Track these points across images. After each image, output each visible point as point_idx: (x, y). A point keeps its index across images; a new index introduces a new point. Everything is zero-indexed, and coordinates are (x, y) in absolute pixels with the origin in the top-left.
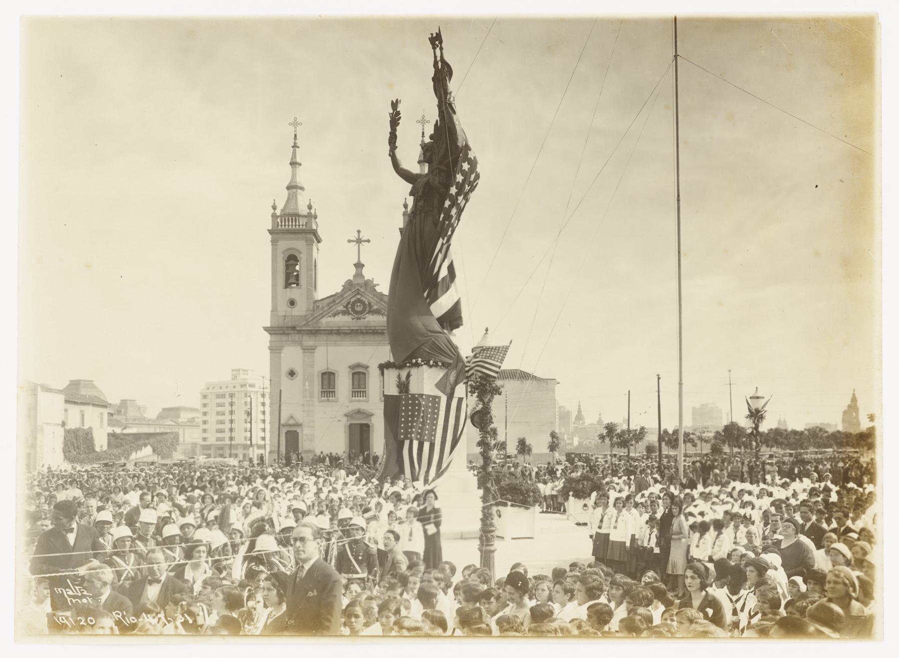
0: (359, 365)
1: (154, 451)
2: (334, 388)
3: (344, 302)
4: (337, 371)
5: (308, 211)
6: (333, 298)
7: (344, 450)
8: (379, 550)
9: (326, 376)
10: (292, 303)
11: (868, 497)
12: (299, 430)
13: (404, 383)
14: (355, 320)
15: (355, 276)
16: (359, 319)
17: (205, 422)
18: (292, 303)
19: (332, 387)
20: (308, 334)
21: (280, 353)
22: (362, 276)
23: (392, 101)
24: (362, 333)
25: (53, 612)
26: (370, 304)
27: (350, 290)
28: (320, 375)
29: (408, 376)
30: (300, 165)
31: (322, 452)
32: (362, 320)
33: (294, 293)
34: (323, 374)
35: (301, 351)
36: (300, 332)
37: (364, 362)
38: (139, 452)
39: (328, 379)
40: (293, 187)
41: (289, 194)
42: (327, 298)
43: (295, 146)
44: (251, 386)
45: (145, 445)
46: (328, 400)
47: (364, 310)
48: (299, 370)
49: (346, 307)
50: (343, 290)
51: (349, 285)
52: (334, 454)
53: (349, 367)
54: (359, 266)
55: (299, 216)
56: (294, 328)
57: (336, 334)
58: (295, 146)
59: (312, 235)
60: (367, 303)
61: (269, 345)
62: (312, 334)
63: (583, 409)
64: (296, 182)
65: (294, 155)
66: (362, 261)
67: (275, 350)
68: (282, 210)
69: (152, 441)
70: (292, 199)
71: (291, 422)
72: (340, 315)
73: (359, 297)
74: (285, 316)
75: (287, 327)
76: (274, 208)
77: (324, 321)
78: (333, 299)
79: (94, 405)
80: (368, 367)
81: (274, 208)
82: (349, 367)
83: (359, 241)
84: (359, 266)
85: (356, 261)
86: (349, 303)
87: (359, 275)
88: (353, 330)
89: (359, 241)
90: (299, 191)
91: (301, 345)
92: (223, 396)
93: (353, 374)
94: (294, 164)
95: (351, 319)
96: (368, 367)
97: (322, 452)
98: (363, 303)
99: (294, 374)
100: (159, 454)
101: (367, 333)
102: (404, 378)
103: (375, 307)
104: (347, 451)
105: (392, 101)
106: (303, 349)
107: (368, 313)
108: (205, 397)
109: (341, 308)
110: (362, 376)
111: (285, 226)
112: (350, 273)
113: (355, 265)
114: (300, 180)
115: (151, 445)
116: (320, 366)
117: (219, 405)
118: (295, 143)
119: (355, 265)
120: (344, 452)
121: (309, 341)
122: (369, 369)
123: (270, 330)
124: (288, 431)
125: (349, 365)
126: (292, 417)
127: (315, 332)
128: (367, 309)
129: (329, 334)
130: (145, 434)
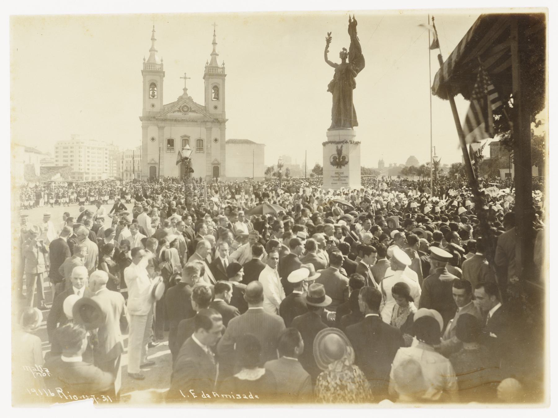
0: (185, 136)
1: (61, 175)
2: (203, 147)
3: (179, 106)
4: (204, 139)
5: (161, 62)
6: (172, 104)
7: (178, 175)
8: (333, 217)
9: (198, 141)
10: (153, 106)
11: (310, 198)
12: (219, 166)
13: (339, 150)
14: (183, 115)
15: (184, 94)
16: (186, 114)
17: (88, 161)
18: (153, 106)
19: (201, 146)
20: (161, 121)
21: (147, 129)
22: (187, 94)
23: (328, 33)
24: (187, 121)
25: (131, 248)
26: (190, 108)
27: (182, 101)
28: (196, 141)
29: (342, 147)
30: (156, 40)
31: (168, 177)
32: (187, 115)
33: (154, 101)
34: (197, 140)
35: (158, 129)
36: (157, 119)
37: (188, 134)
38: (55, 176)
39: (171, 142)
40: (152, 50)
41: (151, 54)
42: (170, 104)
43: (154, 31)
44: (82, 143)
45: (57, 173)
46: (171, 152)
47: (182, 109)
48: (156, 137)
49: (179, 108)
50: (178, 101)
51: (181, 98)
52: (174, 178)
53: (181, 137)
54: (185, 90)
55: (157, 64)
56: (154, 117)
57: (174, 121)
58: (154, 31)
59: (161, 73)
60: (189, 107)
61: (142, 125)
62: (163, 120)
63: (441, 161)
64: (154, 48)
65: (153, 36)
66: (187, 87)
67: (144, 128)
68: (148, 61)
69: (60, 170)
70: (152, 56)
71: (153, 162)
72: (176, 112)
73: (185, 104)
74: (150, 112)
75: (151, 117)
76: (144, 60)
77: (169, 115)
78: (173, 105)
79: (35, 153)
80: (190, 137)
81: (144, 60)
82: (181, 137)
83: (185, 78)
84: (185, 90)
85: (184, 87)
86: (181, 107)
87: (185, 94)
88: (183, 119)
89: (185, 78)
90: (156, 52)
91: (158, 126)
92: (67, 148)
93: (183, 140)
94: (153, 39)
95: (181, 114)
96: (190, 137)
97: (168, 177)
98: (187, 107)
99: (215, 140)
100: (63, 177)
101: (189, 121)
102: (339, 147)
103: (193, 109)
104: (180, 176)
105: (328, 33)
106: (159, 128)
107: (190, 112)
108: (57, 148)
109: (177, 109)
110: (187, 141)
111: (150, 69)
112: (181, 93)
113: (183, 89)
114: (156, 48)
115: (60, 173)
116: (167, 136)
117: (64, 152)
118: (153, 30)
119: (183, 89)
120: (178, 176)
121: (161, 124)
122: (190, 138)
123: (141, 119)
124: (151, 167)
125: (181, 135)
126: (153, 160)
127: (165, 120)
128: (189, 110)
129: (171, 121)
130: (52, 167)
